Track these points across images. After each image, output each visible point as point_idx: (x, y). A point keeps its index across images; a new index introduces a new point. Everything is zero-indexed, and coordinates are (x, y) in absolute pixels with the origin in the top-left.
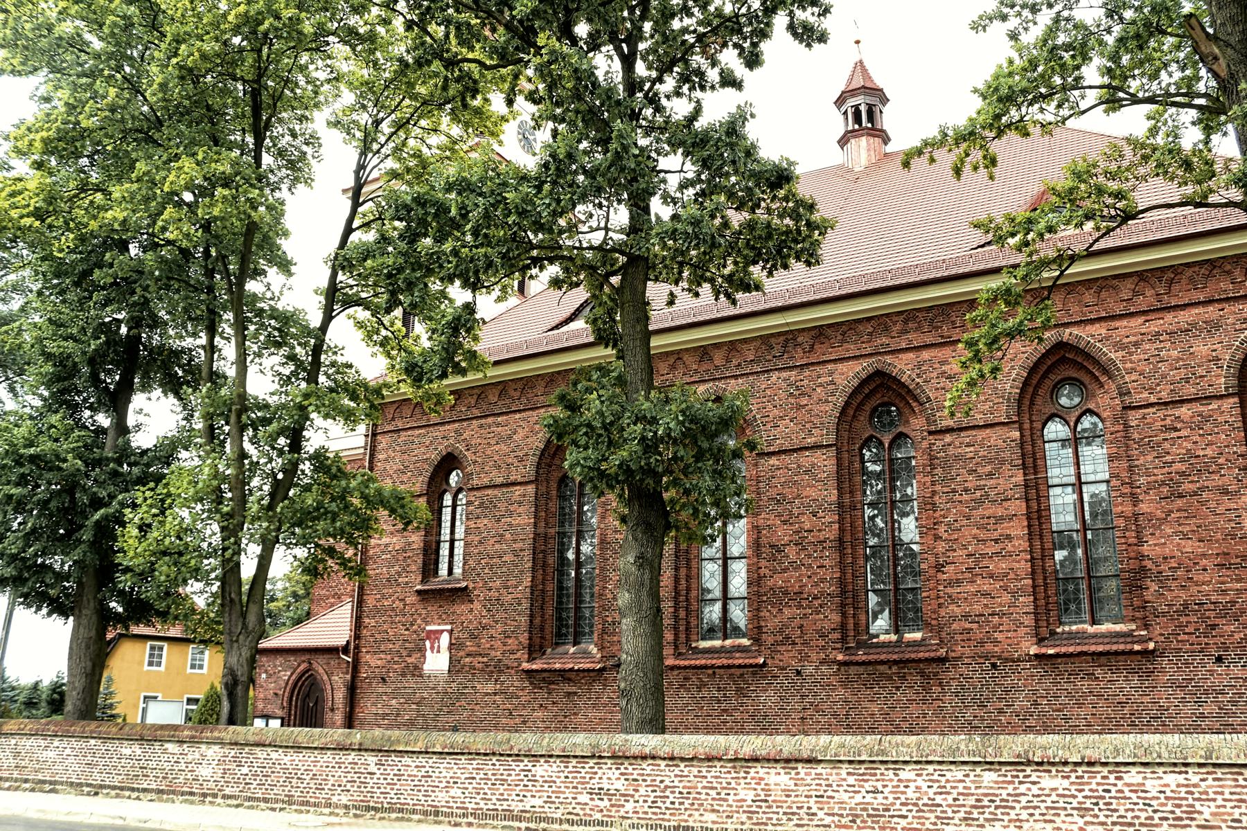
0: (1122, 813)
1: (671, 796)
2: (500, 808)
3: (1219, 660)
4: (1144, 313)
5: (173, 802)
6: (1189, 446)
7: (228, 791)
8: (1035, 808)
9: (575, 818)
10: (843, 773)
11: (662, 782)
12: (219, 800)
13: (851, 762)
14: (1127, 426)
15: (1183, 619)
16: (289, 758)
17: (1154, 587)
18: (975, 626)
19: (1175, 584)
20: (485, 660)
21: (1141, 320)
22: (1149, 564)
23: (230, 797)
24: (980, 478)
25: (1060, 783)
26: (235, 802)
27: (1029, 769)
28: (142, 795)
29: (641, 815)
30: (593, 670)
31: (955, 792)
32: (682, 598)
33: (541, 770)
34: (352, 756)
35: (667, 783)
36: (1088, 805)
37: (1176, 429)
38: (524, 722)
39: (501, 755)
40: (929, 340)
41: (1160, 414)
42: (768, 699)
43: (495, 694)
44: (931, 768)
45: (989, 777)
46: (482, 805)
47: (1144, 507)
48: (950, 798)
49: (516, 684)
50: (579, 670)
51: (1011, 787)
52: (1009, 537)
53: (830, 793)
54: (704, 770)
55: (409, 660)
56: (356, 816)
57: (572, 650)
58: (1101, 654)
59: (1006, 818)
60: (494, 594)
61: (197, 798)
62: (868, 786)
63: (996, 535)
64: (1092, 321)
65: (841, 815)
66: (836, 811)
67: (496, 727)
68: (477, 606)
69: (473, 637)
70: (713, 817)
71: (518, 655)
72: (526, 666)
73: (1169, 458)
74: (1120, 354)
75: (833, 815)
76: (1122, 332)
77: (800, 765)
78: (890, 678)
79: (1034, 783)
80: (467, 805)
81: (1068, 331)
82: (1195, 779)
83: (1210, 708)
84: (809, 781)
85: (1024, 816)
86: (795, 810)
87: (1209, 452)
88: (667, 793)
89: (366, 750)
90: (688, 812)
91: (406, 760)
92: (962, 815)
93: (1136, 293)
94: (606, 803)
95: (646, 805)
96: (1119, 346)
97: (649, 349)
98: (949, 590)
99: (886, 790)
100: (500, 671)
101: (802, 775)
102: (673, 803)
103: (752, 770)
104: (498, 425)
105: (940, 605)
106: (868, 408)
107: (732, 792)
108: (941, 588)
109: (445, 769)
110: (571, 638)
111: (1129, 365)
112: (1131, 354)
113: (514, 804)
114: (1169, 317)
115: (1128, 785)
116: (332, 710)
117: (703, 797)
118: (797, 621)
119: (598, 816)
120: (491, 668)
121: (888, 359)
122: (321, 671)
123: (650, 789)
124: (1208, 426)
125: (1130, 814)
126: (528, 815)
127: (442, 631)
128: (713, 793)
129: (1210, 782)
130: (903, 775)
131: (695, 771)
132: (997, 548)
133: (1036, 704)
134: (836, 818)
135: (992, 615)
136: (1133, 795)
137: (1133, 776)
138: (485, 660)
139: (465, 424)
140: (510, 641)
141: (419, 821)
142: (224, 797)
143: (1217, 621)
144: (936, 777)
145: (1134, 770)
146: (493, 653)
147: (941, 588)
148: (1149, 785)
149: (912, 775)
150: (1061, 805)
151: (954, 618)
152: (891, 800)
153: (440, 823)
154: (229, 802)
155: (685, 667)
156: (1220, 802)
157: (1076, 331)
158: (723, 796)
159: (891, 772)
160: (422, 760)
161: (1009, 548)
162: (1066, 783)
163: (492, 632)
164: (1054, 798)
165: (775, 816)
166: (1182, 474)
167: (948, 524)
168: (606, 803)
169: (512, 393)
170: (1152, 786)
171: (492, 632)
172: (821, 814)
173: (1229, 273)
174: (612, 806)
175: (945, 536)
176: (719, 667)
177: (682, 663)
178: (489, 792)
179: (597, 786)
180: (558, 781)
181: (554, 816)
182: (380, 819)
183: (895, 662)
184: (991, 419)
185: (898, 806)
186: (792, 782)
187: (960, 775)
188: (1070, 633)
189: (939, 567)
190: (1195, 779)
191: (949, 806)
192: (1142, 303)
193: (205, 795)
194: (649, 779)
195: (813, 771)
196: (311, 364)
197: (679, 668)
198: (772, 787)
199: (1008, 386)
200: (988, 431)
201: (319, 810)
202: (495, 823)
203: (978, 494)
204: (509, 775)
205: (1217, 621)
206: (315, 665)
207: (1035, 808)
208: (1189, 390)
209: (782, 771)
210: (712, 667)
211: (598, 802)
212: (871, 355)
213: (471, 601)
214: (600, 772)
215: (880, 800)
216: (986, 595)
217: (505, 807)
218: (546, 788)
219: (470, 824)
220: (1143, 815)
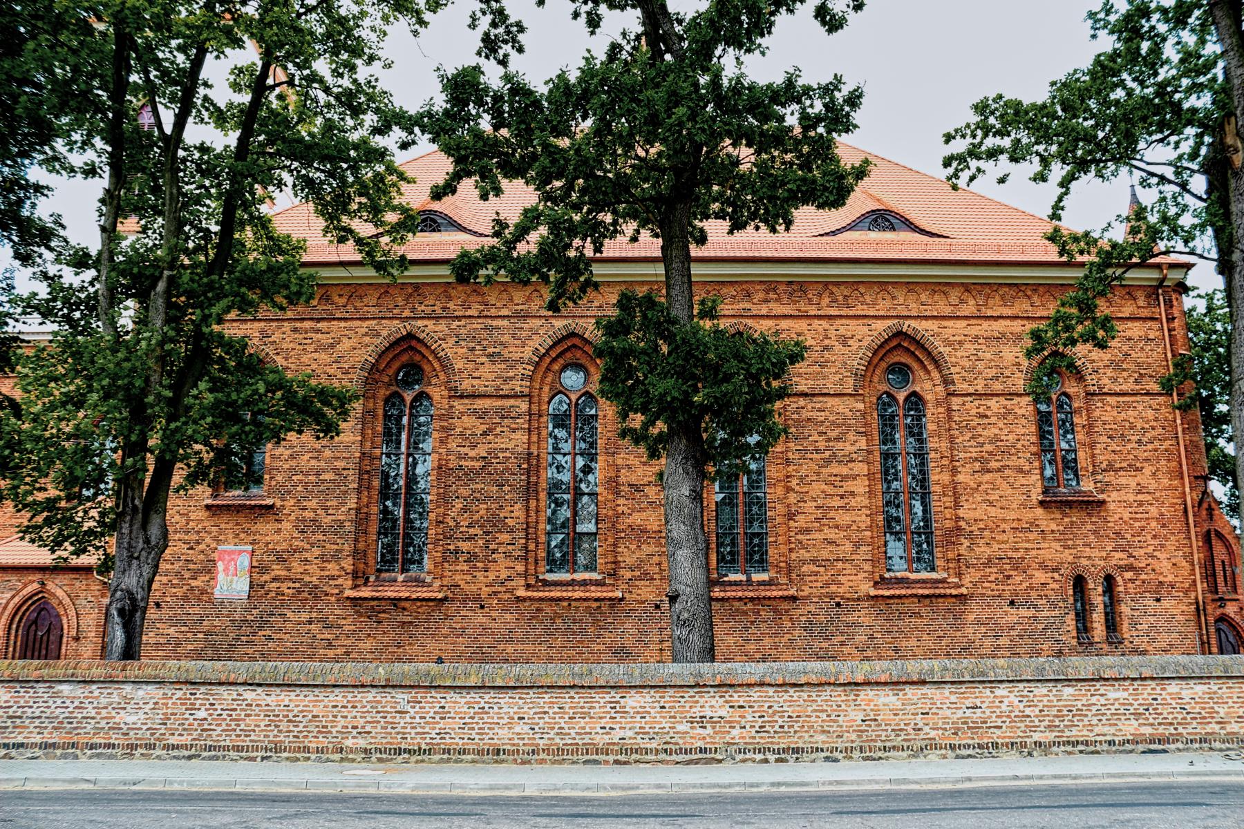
0: (1165, 715)
1: (780, 720)
2: (580, 742)
3: (1012, 603)
4: (966, 318)
5: (76, 757)
6: (997, 431)
7: (173, 740)
8: (1103, 715)
9: (673, 747)
10: (947, 692)
11: (770, 707)
12: (158, 752)
13: (953, 683)
14: (949, 410)
15: (988, 570)
16: (273, 697)
17: (966, 543)
18: (822, 569)
19: (982, 541)
20: (297, 585)
21: (964, 323)
22: (963, 524)
23: (174, 747)
24: (829, 440)
25: (1121, 695)
26: (187, 753)
27: (1098, 684)
28: (13, 753)
29: (748, 740)
30: (435, 600)
31: (1041, 704)
32: (531, 530)
33: (633, 701)
34: (372, 694)
35: (776, 708)
36: (1141, 711)
37: (986, 417)
38: (347, 653)
39: (583, 687)
40: (787, 310)
41: (976, 403)
42: (628, 631)
43: (310, 623)
44: (1021, 685)
45: (1068, 691)
46: (557, 740)
47: (960, 478)
48: (1037, 710)
49: (337, 612)
50: (417, 599)
51: (1084, 699)
52: (853, 494)
53: (934, 711)
54: (814, 695)
55: (194, 583)
56: (380, 760)
57: (401, 578)
58: (927, 596)
59: (1080, 724)
60: (308, 515)
61: (119, 751)
62: (968, 703)
63: (841, 491)
64: (926, 318)
65: (945, 729)
66: (940, 725)
67: (311, 658)
68: (286, 525)
69: (280, 559)
70: (823, 737)
71: (340, 581)
72: (348, 593)
73: (981, 440)
74: (948, 349)
75: (937, 729)
76: (950, 331)
77: (907, 687)
78: (745, 613)
79: (1102, 695)
80: (538, 741)
81: (907, 323)
82: (1215, 688)
83: (1004, 641)
84: (915, 701)
85: (1095, 722)
86: (902, 726)
87: (1011, 438)
88: (776, 718)
89: (394, 687)
90: (798, 735)
91: (451, 696)
92: (1047, 723)
93: (962, 301)
94: (709, 731)
95: (753, 730)
96: (947, 342)
97: (690, 276)
98: (799, 537)
99: (984, 706)
100: (316, 598)
101: (910, 696)
102: (782, 727)
103: (862, 693)
104: (318, 331)
105: (791, 550)
106: (884, 365)
107: (842, 714)
108: (792, 534)
109: (508, 704)
110: (398, 566)
111: (953, 360)
112: (955, 350)
113: (598, 737)
114: (985, 324)
115: (1169, 694)
116: (77, 639)
117: (813, 719)
118: (656, 559)
119: (700, 744)
120: (306, 595)
121: (750, 322)
122: (60, 593)
123: (757, 715)
124: (1010, 417)
125: (1170, 716)
126: (616, 748)
127: (240, 552)
128: (824, 716)
129: (1224, 690)
130: (998, 692)
131: (805, 695)
132: (841, 503)
133: (872, 637)
134: (940, 732)
135: (837, 560)
136: (1173, 702)
137: (1173, 687)
138: (297, 585)
139: (274, 324)
140: (329, 566)
141: (473, 761)
142: (167, 747)
143: (1012, 573)
144: (1025, 693)
145: (1174, 682)
146: (307, 579)
147: (792, 534)
148: (1184, 693)
149: (1005, 693)
150: (1122, 711)
151: (804, 562)
152: (988, 713)
153: (502, 761)
154: (176, 753)
155: (541, 599)
156: (1231, 704)
157: (913, 323)
158: (833, 717)
159: (988, 691)
160: (474, 696)
161: (853, 504)
162: (1125, 694)
163: (308, 555)
164: (1117, 706)
165: (884, 733)
166: (990, 453)
167: (801, 478)
168: (709, 731)
169: (336, 299)
170: (1186, 694)
171: (308, 555)
172: (927, 729)
173: (1029, 297)
174: (716, 733)
175: (797, 488)
176: (576, 600)
177: (536, 594)
178: (566, 726)
179: (698, 715)
180: (551, 711)
181: (648, 746)
182: (417, 762)
183: (752, 599)
184: (839, 389)
185: (994, 719)
186: (899, 703)
187: (1044, 691)
188: (896, 578)
189: (791, 516)
190: (1215, 688)
191: (1037, 716)
192: (967, 310)
193: (133, 747)
194: (756, 705)
195: (919, 692)
196: (235, 208)
197: (531, 599)
198: (881, 707)
199: (855, 363)
200: (837, 399)
201: (324, 757)
202: (575, 758)
203: (827, 454)
204: (591, 708)
205: (1012, 573)
206: (50, 586)
207: (1103, 715)
208: (997, 387)
209: (891, 693)
210: (569, 599)
211: (701, 731)
212: (734, 316)
213: (279, 521)
214: (702, 700)
215: (979, 715)
216: (831, 542)
217: (587, 741)
218: (638, 719)
219: (542, 761)
220: (1180, 716)
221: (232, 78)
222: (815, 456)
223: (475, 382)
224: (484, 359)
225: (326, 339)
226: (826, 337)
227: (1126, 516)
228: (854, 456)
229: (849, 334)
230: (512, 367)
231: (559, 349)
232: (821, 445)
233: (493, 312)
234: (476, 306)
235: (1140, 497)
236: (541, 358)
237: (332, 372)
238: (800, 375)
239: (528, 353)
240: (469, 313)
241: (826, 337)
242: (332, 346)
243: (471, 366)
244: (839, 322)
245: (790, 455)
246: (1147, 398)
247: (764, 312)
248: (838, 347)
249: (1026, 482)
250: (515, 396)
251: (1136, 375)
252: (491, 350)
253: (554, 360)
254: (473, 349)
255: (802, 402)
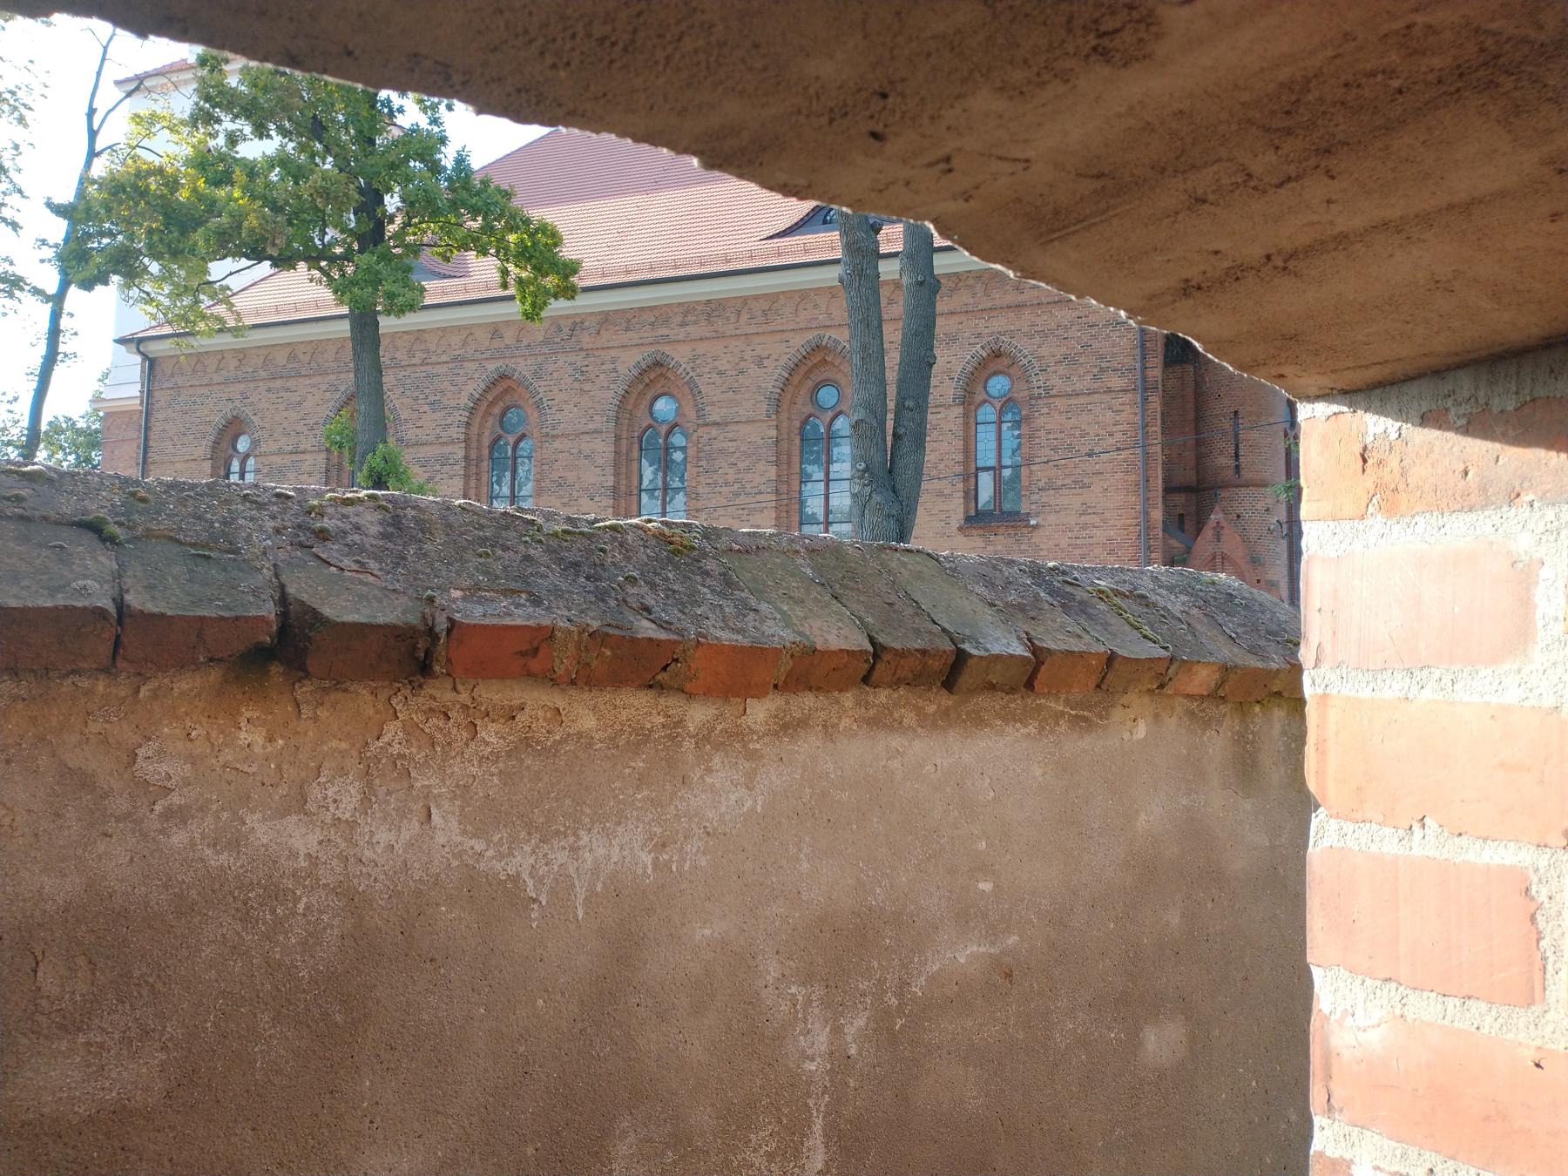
104: (287, 390)
221: (1273, 250)
222: (725, 489)
223: (418, 431)
224: (426, 408)
225: (294, 397)
226: (743, 359)
227: (1064, 542)
228: (763, 488)
229: (765, 354)
230: (449, 414)
231: (495, 392)
232: (731, 478)
233: (434, 359)
234: (419, 354)
235: (1084, 519)
236: (477, 402)
237: (299, 429)
238: (713, 404)
239: (464, 400)
240: (414, 361)
241: (743, 359)
242: (299, 404)
243: (415, 415)
244: (757, 339)
245: (700, 490)
246: (1106, 397)
247: (681, 337)
248: (753, 370)
249: (945, 508)
250: (453, 442)
251: (1095, 370)
252: (432, 398)
253: (492, 404)
254: (417, 398)
255: (714, 432)
